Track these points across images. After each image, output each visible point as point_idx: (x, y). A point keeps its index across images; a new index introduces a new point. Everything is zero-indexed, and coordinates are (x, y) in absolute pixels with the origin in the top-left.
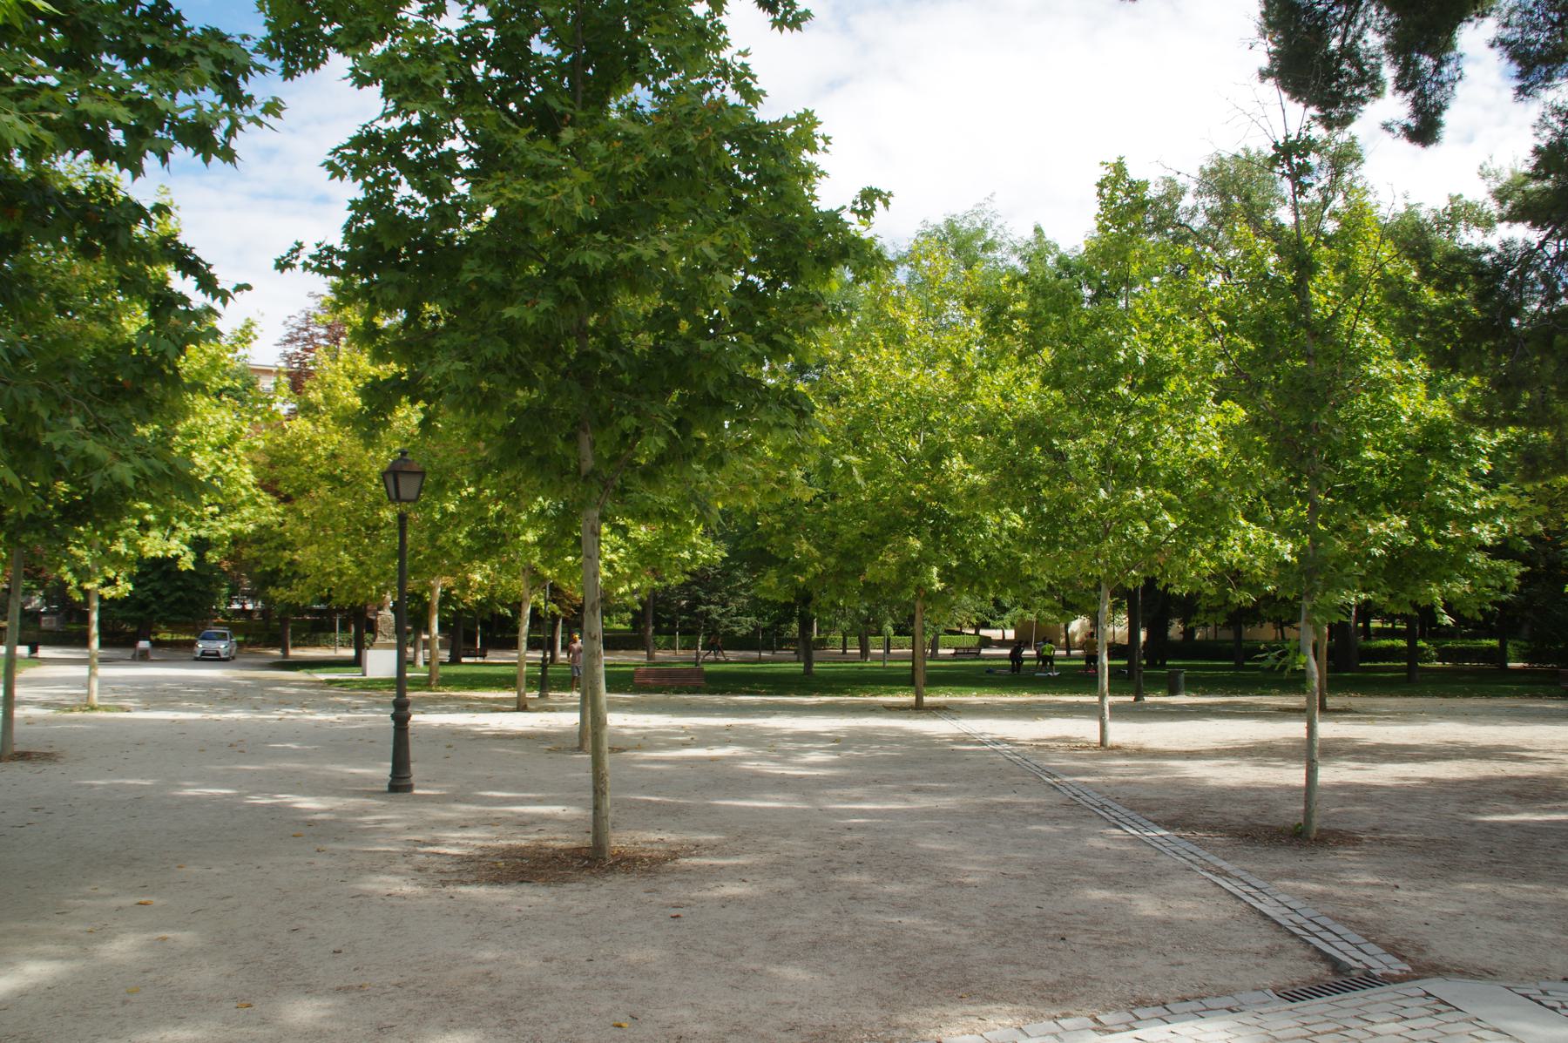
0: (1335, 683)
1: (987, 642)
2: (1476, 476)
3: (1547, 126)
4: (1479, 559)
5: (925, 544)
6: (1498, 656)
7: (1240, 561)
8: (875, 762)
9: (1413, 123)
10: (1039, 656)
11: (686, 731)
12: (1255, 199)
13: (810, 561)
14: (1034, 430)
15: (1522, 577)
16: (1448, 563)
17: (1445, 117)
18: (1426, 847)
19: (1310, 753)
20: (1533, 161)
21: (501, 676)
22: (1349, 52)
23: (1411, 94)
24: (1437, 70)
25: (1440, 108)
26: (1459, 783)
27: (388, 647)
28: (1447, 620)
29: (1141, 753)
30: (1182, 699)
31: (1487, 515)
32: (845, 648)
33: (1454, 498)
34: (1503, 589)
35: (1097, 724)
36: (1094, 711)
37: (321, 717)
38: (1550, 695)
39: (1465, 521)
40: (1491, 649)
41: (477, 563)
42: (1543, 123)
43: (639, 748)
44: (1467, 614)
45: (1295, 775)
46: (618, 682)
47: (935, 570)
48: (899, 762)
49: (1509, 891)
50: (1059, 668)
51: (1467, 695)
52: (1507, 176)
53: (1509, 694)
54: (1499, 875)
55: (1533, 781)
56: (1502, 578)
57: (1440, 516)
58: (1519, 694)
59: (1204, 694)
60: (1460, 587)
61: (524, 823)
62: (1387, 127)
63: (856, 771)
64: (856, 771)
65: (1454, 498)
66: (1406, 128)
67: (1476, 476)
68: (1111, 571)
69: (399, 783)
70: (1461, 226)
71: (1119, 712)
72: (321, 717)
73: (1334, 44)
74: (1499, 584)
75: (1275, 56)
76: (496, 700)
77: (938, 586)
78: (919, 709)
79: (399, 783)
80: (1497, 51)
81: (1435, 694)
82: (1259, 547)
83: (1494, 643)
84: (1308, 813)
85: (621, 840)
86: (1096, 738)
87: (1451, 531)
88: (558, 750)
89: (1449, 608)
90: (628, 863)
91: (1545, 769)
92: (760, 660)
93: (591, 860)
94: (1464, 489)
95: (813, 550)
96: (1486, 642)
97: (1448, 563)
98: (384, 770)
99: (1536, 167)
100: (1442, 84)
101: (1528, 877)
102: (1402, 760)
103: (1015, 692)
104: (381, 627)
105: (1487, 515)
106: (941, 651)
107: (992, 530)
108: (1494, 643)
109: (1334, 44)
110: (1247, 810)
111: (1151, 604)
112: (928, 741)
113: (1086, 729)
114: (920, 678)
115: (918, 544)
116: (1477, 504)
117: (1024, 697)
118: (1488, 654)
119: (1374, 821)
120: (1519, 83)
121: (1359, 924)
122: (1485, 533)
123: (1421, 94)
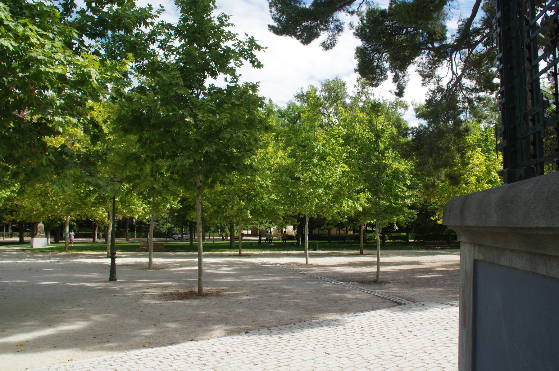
0: (385, 246)
1: (243, 235)
2: (405, 184)
3: (429, 94)
4: (406, 209)
5: (246, 203)
6: (406, 238)
7: (347, 210)
8: (245, 270)
9: (397, 91)
10: (267, 239)
11: (177, 263)
12: (339, 95)
13: (209, 208)
14: (288, 171)
15: (418, 215)
16: (400, 210)
17: (405, 90)
18: (406, 283)
19: (378, 264)
20: (425, 103)
21: (88, 247)
22: (378, 67)
23: (397, 83)
24: (403, 77)
25: (404, 88)
26: (408, 270)
27: (42, 237)
28: (397, 228)
29: (318, 266)
30: (318, 252)
31: (409, 197)
32: (209, 237)
33: (400, 191)
34: (413, 218)
35: (305, 259)
36: (304, 256)
37: (8, 261)
38: (422, 249)
39: (404, 198)
40: (404, 236)
41: (100, 208)
42: (427, 94)
43: (167, 268)
44: (402, 225)
45: (374, 269)
46: (207, 248)
47: (249, 212)
48: (249, 269)
49: (427, 289)
50: (274, 243)
51: (400, 249)
52: (418, 105)
53: (411, 249)
54: (424, 287)
55: (426, 269)
56: (413, 215)
57: (396, 197)
58: (414, 249)
59: (324, 250)
60: (402, 217)
61: (166, 287)
62: (390, 91)
63: (243, 272)
64: (243, 272)
65: (400, 191)
66: (396, 93)
67: (405, 184)
68: (310, 213)
69: (113, 278)
70: (398, 107)
71: (312, 256)
72: (8, 261)
73: (375, 64)
74: (412, 217)
75: (359, 65)
76: (96, 255)
77: (250, 217)
78: (240, 255)
79: (113, 278)
80: (417, 72)
81: (391, 249)
82: (351, 206)
83: (405, 234)
84: (378, 276)
85: (205, 289)
86: (305, 263)
87: (400, 202)
88: (141, 269)
89: (398, 224)
90: (207, 295)
91: (427, 266)
92: (166, 241)
93: (200, 294)
94: (403, 189)
95: (209, 204)
96: (402, 234)
97: (400, 210)
98: (107, 276)
99: (426, 105)
100: (404, 82)
101: (430, 287)
102: (391, 265)
103: (265, 250)
104: (39, 230)
105: (409, 197)
106: (262, 238)
107: (266, 199)
108: (405, 234)
109: (375, 64)
110: (359, 277)
111: (299, 222)
112: (254, 264)
113: (302, 260)
114: (240, 246)
115: (244, 204)
116: (406, 194)
117: (268, 252)
118: (403, 238)
119: (391, 278)
120: (422, 82)
121: (399, 296)
122: (409, 202)
123: (399, 83)
